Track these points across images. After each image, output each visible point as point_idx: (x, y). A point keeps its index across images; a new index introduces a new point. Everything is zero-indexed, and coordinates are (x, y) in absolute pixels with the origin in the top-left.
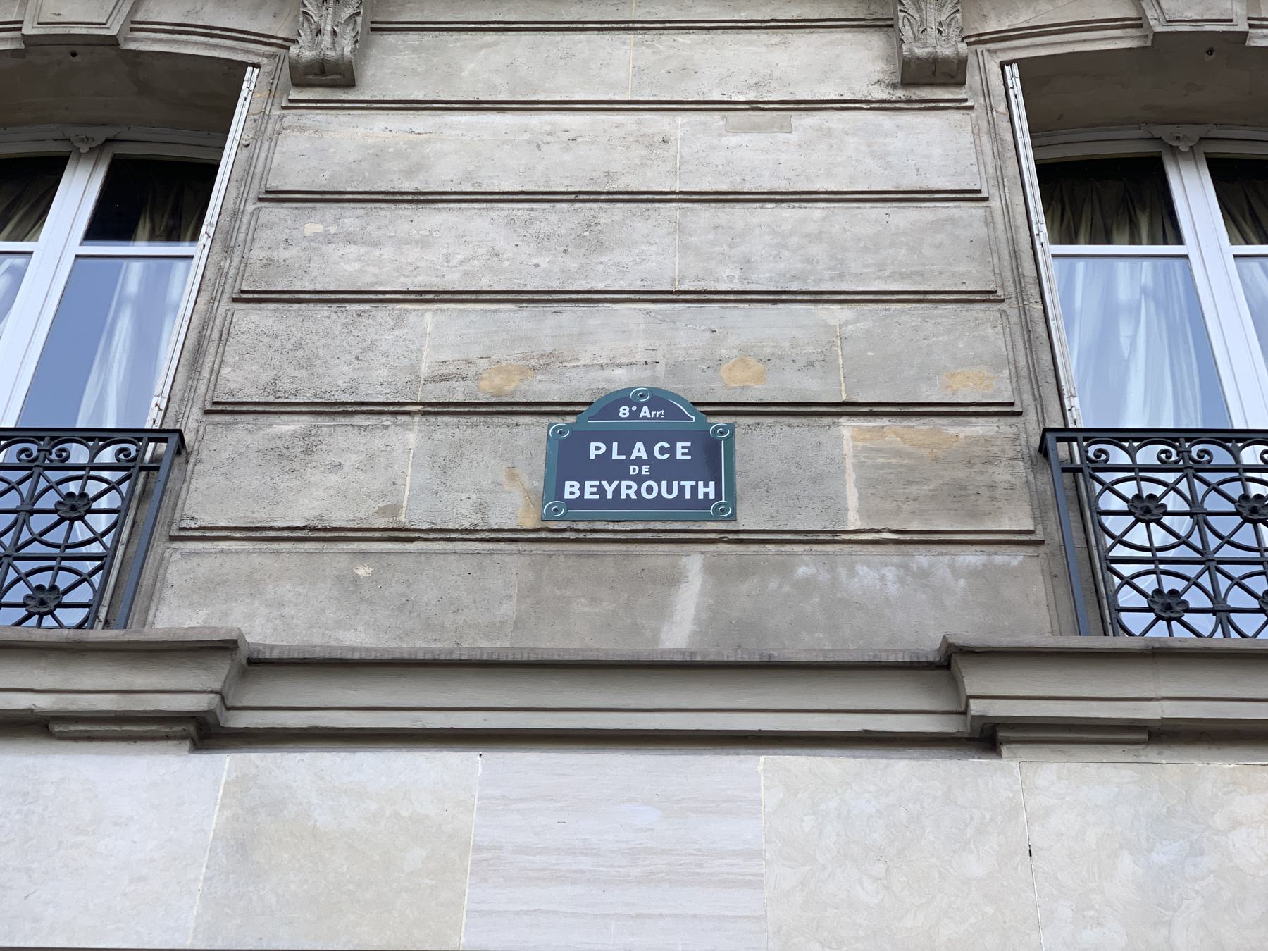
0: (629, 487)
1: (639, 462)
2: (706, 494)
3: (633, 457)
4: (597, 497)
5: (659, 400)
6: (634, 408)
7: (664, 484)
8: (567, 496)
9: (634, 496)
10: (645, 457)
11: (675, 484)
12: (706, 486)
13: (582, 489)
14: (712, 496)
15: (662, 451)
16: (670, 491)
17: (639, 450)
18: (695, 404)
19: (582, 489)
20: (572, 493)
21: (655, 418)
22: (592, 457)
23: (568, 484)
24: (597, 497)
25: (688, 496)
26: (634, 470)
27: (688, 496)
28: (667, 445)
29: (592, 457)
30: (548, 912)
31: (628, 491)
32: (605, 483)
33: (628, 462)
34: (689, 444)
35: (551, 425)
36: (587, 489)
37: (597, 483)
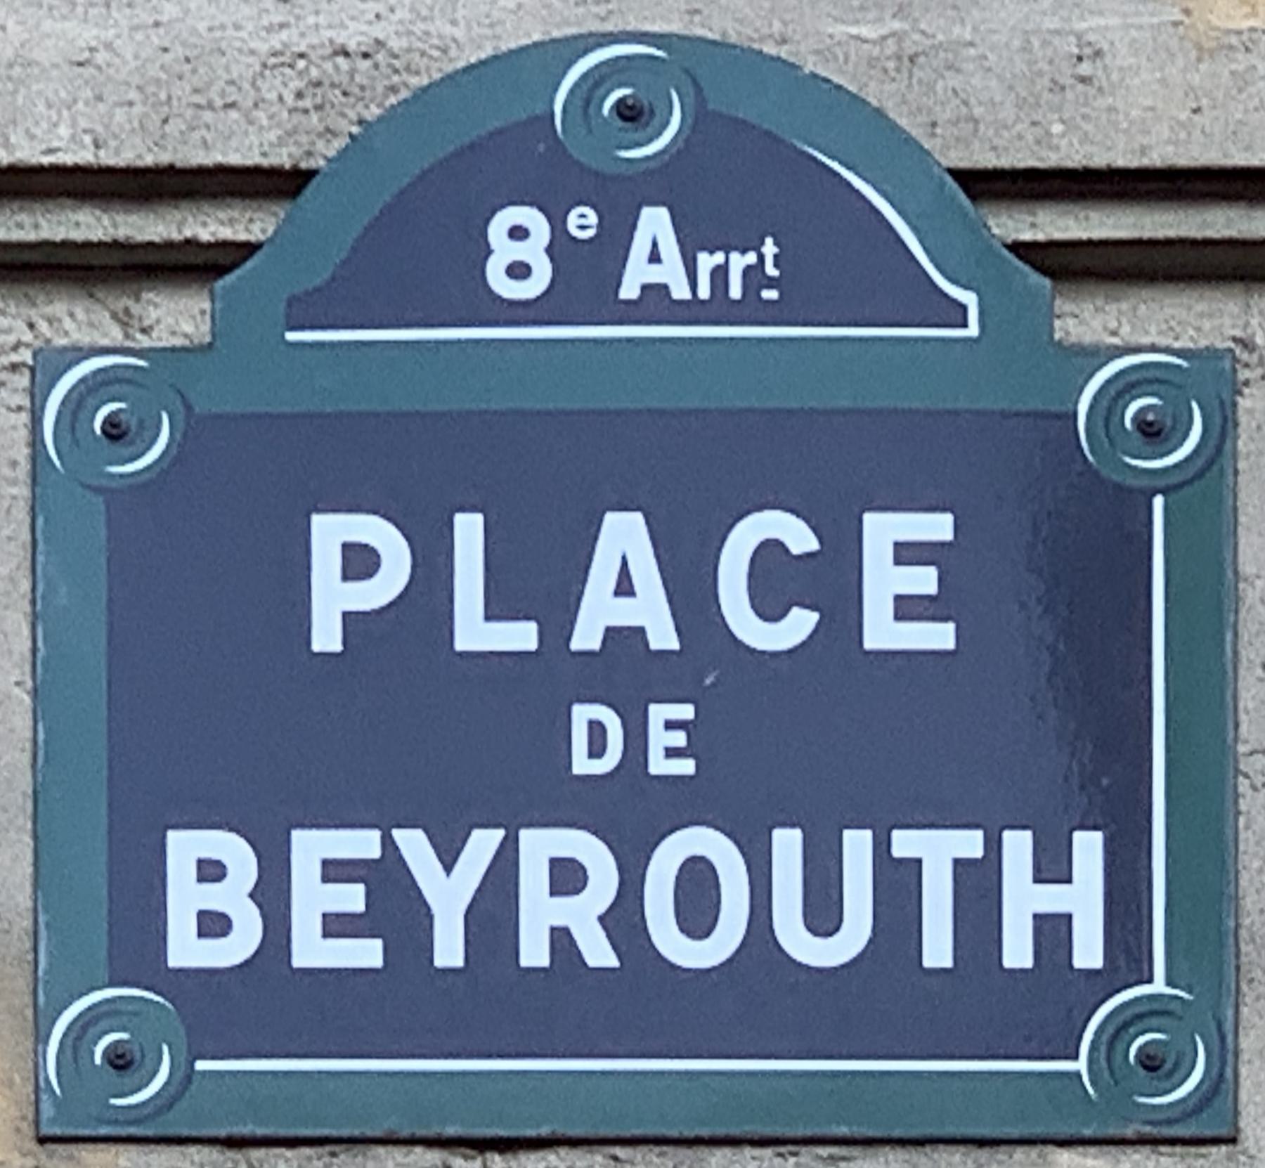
0: (567, 877)
1: (625, 670)
2: (1053, 931)
3: (586, 637)
4: (366, 953)
5: (750, 150)
6: (583, 222)
7: (787, 845)
8: (186, 949)
9: (598, 952)
10: (663, 636)
11: (857, 845)
12: (1052, 866)
13: (272, 894)
14: (1088, 951)
15: (770, 593)
16: (823, 914)
17: (623, 585)
18: (985, 185)
19: (272, 894)
20: (213, 925)
21: (717, 308)
22: (326, 636)
23: (184, 848)
24: (366, 953)
25: (938, 949)
26: (592, 738)
27: (938, 949)
28: (799, 537)
29: (326, 636)
30: (103, 268)
31: (565, 911)
32: (414, 844)
33: (555, 676)
34: (938, 527)
35: (46, 366)
36: (312, 898)
37: (363, 844)
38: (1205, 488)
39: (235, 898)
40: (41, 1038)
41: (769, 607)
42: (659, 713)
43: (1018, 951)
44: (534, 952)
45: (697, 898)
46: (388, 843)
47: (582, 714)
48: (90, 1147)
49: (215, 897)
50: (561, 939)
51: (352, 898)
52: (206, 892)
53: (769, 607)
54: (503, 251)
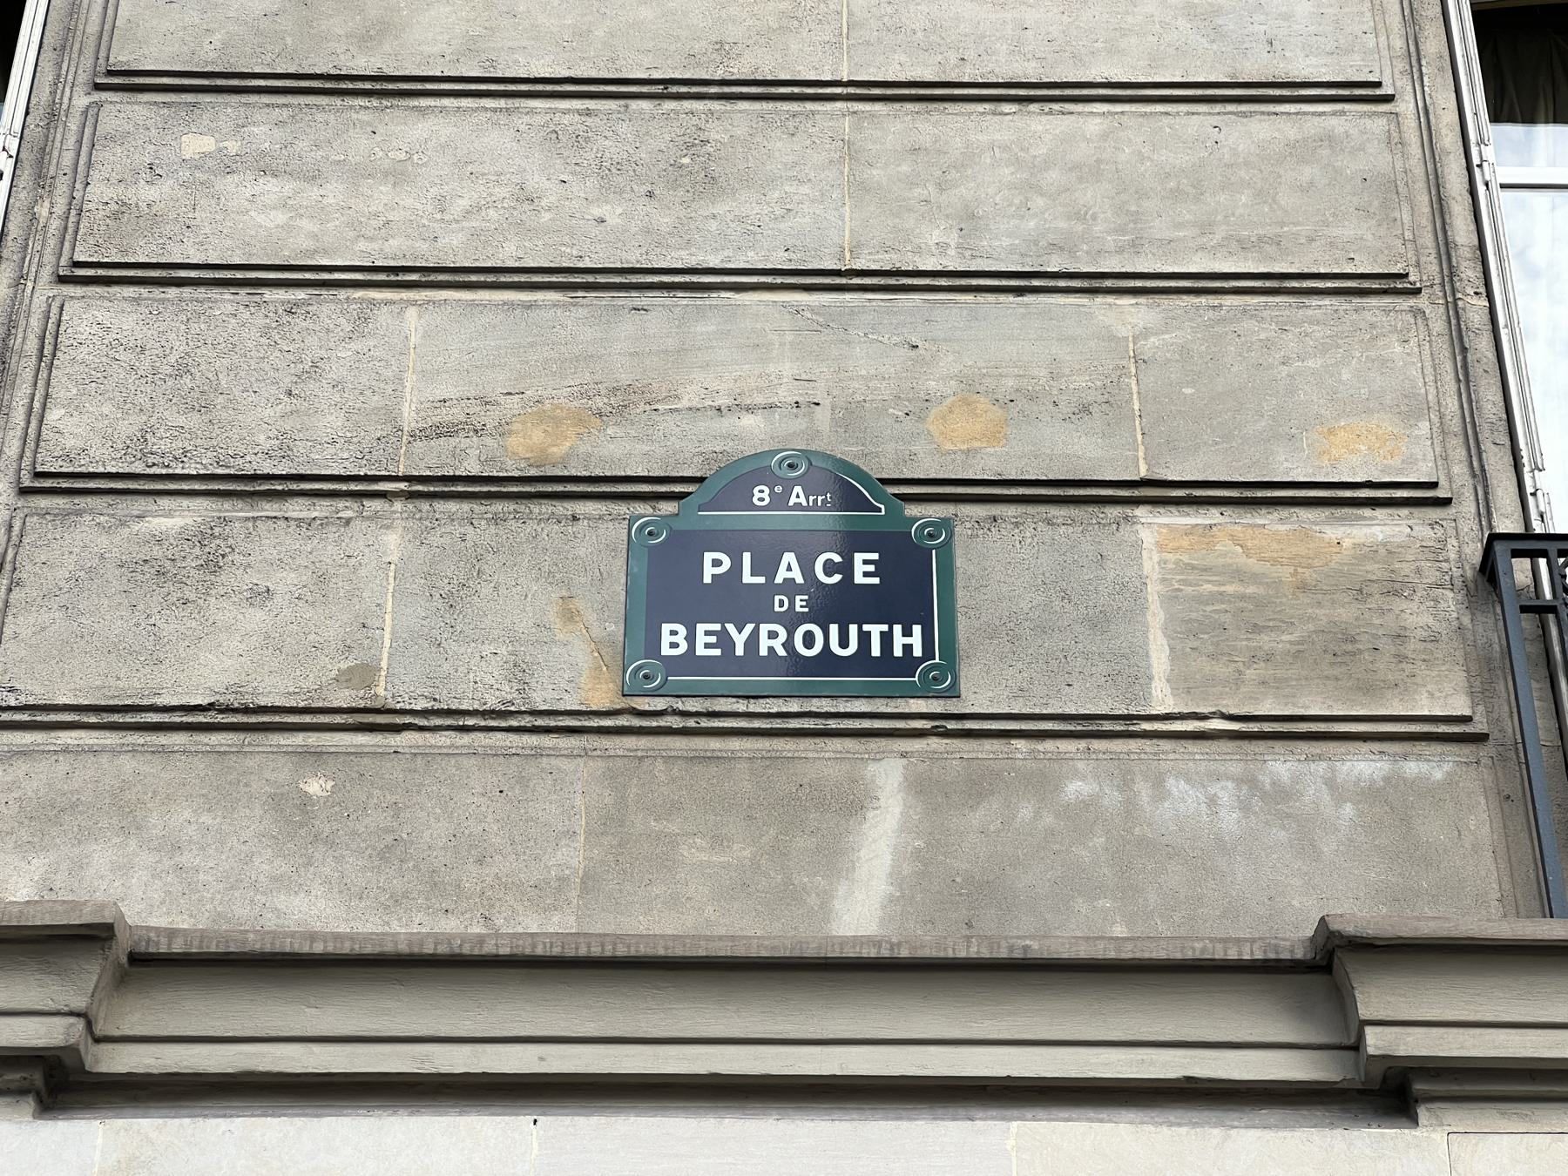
1: (789, 587)
2: (908, 648)
3: (779, 580)
4: (717, 652)
6: (778, 489)
7: (834, 629)
8: (666, 651)
9: (781, 652)
11: (853, 629)
12: (907, 633)
13: (691, 638)
14: (917, 652)
15: (830, 568)
16: (844, 643)
17: (789, 568)
19: (691, 638)
22: (707, 579)
23: (666, 628)
24: (717, 652)
25: (876, 651)
26: (780, 604)
27: (876, 651)
28: (837, 558)
29: (707, 579)
31: (772, 643)
32: (730, 627)
33: (771, 588)
36: (701, 639)
37: (717, 627)
38: (946, 550)
39: (680, 639)
40: (624, 672)
41: (828, 574)
42: (798, 598)
43: (898, 652)
44: (763, 652)
45: (809, 640)
46: (723, 627)
47: (777, 598)
48: (1492, 344)
49: (674, 639)
50: (771, 649)
51: (713, 639)
52: (672, 639)
53: (828, 574)
54: (757, 495)
